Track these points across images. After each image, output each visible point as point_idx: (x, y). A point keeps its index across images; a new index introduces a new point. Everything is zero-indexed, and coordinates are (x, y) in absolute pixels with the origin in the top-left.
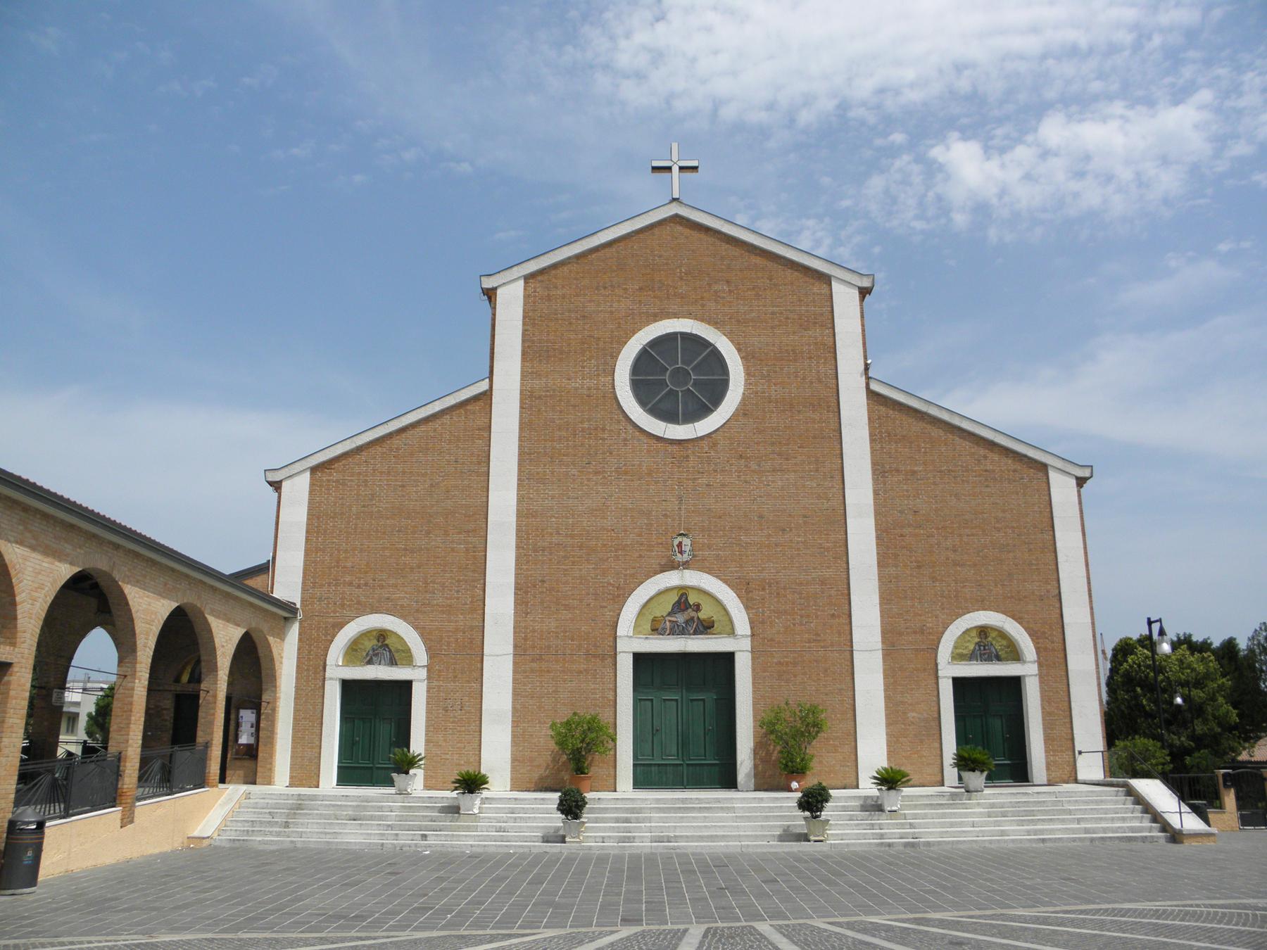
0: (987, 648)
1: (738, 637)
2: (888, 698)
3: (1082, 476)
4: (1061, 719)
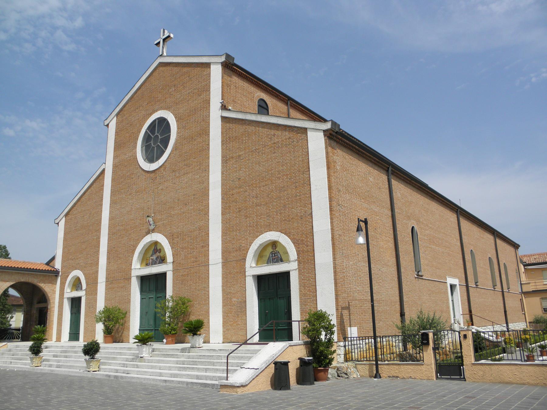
0: (276, 255)
1: (168, 263)
2: (223, 290)
3: (326, 128)
4: (311, 298)
